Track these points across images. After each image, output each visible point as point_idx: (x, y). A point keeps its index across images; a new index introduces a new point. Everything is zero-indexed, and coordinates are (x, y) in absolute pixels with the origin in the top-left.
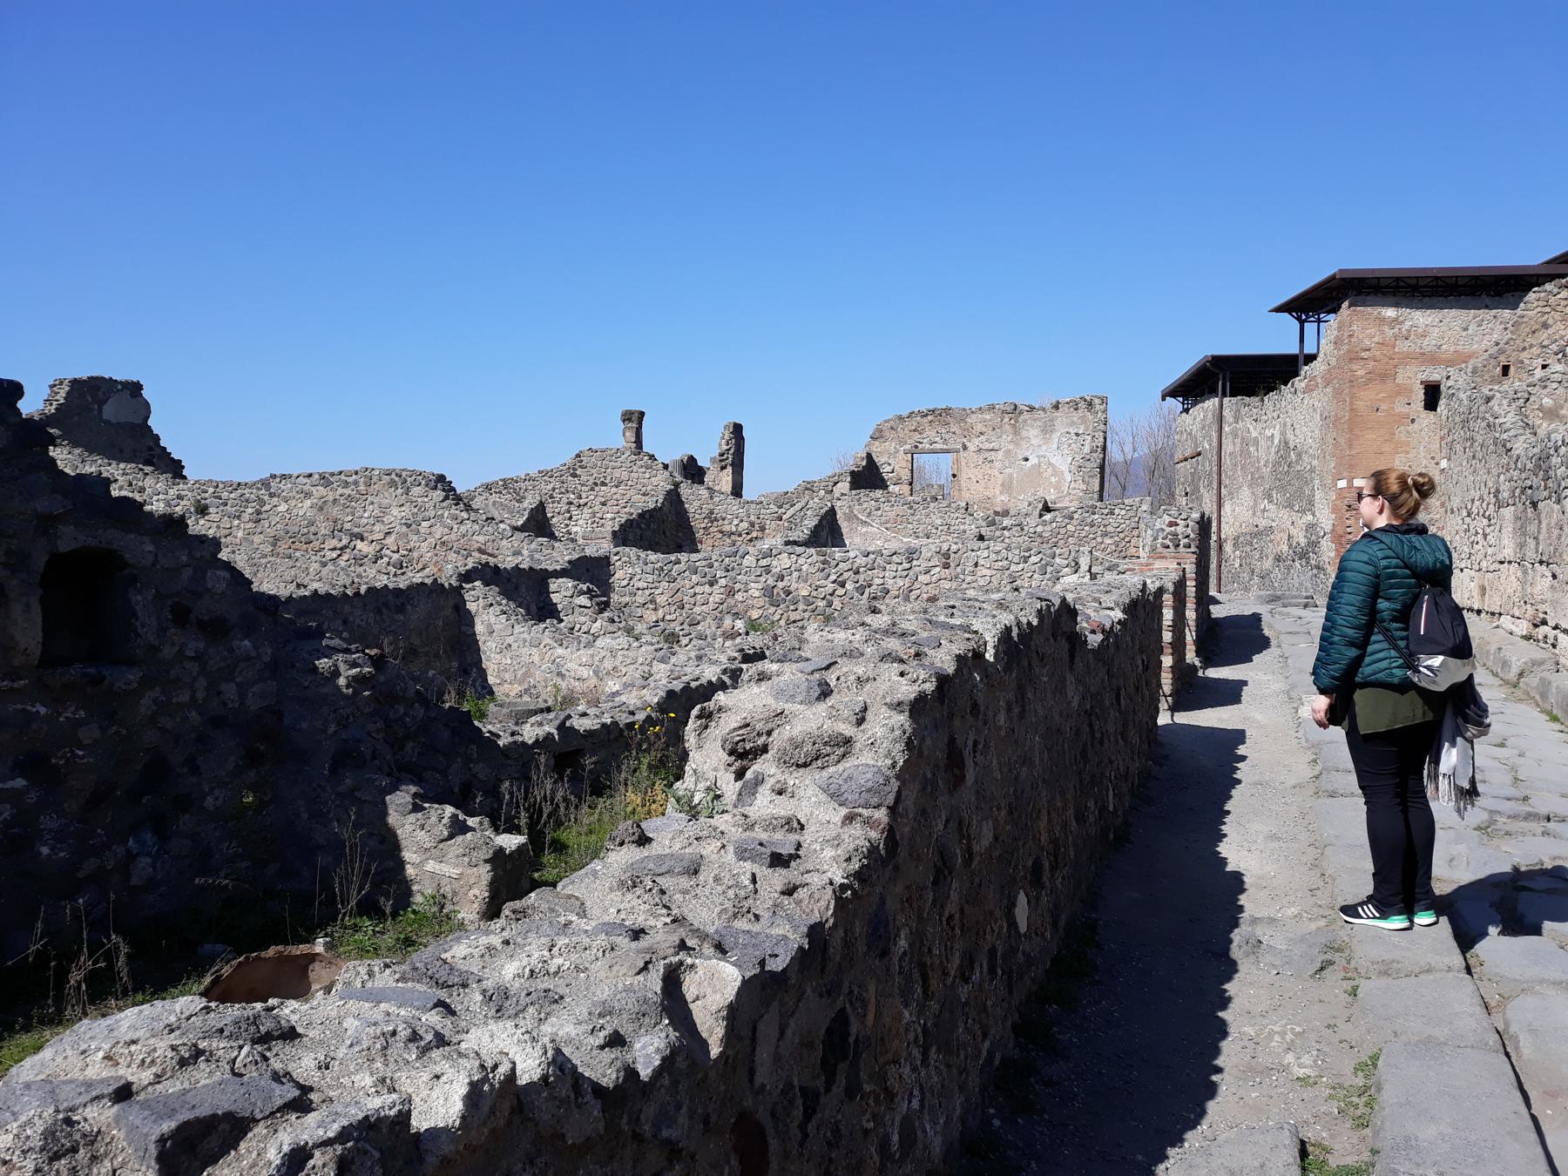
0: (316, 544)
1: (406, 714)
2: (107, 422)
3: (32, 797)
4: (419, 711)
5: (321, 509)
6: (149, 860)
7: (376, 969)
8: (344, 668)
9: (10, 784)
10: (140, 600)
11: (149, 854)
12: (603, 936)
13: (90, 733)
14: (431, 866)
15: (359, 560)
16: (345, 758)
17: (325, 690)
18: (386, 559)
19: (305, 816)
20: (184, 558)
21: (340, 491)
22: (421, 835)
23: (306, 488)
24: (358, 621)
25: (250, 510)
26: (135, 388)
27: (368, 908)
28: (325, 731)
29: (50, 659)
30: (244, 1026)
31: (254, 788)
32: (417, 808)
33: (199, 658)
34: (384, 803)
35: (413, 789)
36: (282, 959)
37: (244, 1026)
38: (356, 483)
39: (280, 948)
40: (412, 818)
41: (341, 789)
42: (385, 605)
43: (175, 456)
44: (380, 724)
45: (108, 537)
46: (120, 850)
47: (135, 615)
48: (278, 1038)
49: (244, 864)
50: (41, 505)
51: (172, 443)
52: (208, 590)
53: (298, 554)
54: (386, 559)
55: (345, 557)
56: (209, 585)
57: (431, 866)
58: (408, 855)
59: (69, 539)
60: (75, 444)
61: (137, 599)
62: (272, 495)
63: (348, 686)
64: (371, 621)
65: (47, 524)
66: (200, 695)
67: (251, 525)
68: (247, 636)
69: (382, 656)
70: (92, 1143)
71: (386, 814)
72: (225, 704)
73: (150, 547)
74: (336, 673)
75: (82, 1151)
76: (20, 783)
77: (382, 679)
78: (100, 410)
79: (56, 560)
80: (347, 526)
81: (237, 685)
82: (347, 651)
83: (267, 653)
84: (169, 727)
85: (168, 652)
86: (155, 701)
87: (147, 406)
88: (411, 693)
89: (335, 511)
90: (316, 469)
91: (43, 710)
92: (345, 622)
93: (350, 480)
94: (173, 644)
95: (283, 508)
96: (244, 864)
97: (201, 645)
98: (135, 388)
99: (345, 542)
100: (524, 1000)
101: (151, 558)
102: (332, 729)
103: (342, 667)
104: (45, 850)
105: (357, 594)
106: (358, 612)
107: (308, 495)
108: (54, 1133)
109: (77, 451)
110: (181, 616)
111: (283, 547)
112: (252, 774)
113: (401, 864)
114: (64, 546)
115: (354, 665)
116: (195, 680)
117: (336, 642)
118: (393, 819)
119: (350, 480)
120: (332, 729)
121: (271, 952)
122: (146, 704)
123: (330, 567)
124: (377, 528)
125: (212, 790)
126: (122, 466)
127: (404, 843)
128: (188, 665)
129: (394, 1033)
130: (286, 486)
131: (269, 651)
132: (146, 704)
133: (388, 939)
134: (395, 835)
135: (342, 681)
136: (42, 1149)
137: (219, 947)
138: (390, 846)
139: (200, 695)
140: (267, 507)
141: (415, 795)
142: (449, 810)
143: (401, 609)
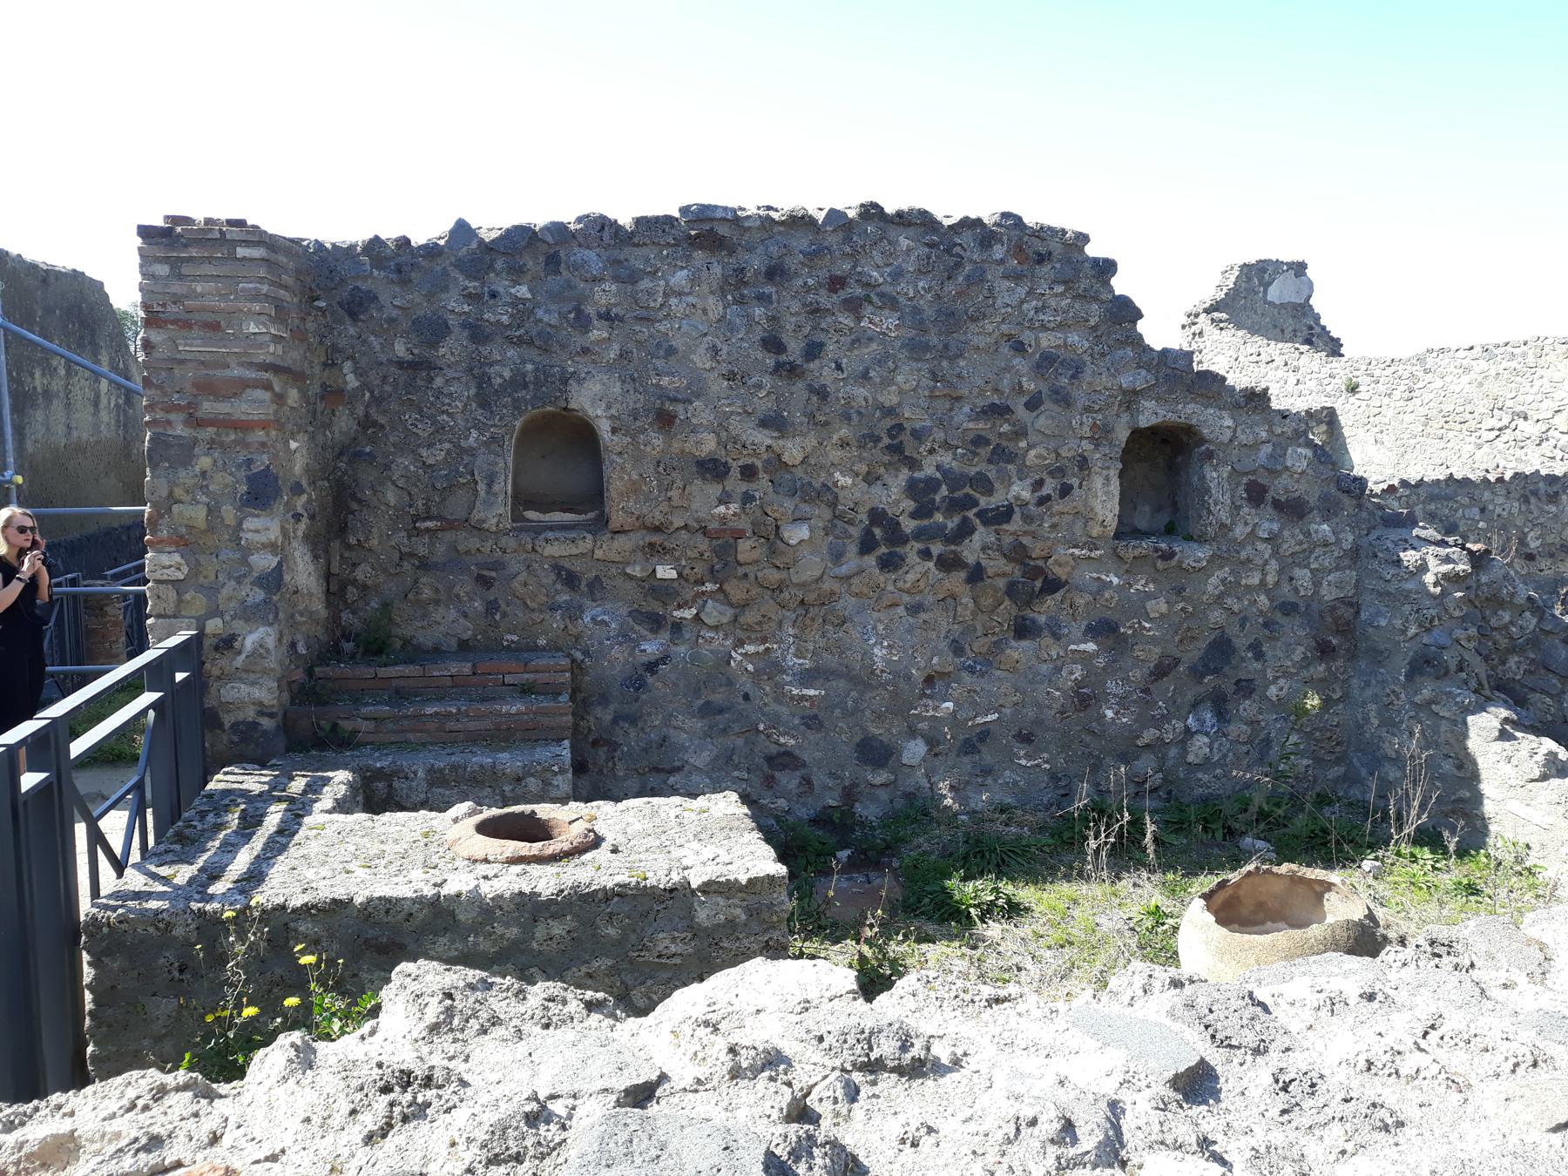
0: (1472, 424)
1: (1511, 622)
2: (1271, 303)
3: (1101, 662)
4: (1530, 621)
5: (1481, 384)
6: (1206, 740)
7: (1157, 984)
8: (1433, 562)
9: (1082, 647)
10: (1215, 477)
11: (1207, 734)
12: (1533, 1033)
13: (1158, 606)
14: (1514, 806)
15: (1520, 444)
16: (1425, 664)
17: (1409, 586)
18: (1552, 442)
19: (1376, 722)
20: (1264, 434)
21: (1505, 364)
22: (1508, 769)
23: (1465, 362)
24: (1499, 510)
25: (1402, 388)
26: (1300, 268)
27: (1429, 838)
28: (1404, 632)
29: (1126, 531)
30: (851, 1040)
31: (1321, 685)
32: (1504, 736)
33: (1272, 539)
34: (1465, 723)
35: (1504, 713)
36: (1294, 879)
37: (851, 1040)
38: (1524, 355)
39: (1294, 867)
40: (1499, 745)
41: (1418, 699)
42: (1535, 493)
43: (1334, 334)
44: (1473, 631)
45: (1190, 412)
46: (1179, 725)
47: (1208, 491)
48: (892, 1070)
49: (1305, 762)
50: (1125, 381)
51: (1332, 322)
52: (1287, 468)
53: (1451, 434)
54: (1552, 442)
55: (1504, 438)
56: (1289, 464)
57: (1514, 806)
58: (1486, 787)
59: (1150, 414)
60: (1239, 327)
61: (1211, 474)
62: (1427, 371)
63: (1436, 584)
64: (1515, 511)
65: (1130, 399)
66: (1271, 579)
67: (1402, 403)
68: (1326, 520)
69: (1488, 552)
70: (543, 1157)
71: (1465, 736)
72: (1296, 590)
73: (1229, 422)
74: (1423, 568)
75: (527, 1164)
76: (1091, 647)
77: (1484, 579)
78: (1265, 292)
79: (1137, 434)
80: (1509, 403)
81: (1312, 571)
82: (1442, 544)
83: (1348, 539)
84: (1236, 608)
85: (1240, 532)
86: (1223, 581)
87: (1310, 284)
88: (1520, 599)
89: (1494, 388)
90: (1477, 342)
91: (1115, 581)
92: (1483, 510)
93: (1516, 351)
94: (1246, 524)
95: (1439, 383)
96: (1305, 762)
97: (1275, 527)
98: (1300, 268)
99: (1505, 422)
100: (1337, 1108)
101: (1229, 434)
102: (1413, 631)
103: (1432, 562)
104: (1110, 714)
105: (1500, 480)
106: (1501, 500)
107: (1467, 370)
108: (504, 1130)
109: (1241, 333)
110: (1256, 494)
111: (1436, 425)
112: (1322, 668)
113: (1478, 798)
114: (1144, 422)
115: (1447, 560)
116: (1266, 563)
117: (1431, 533)
118: (1475, 744)
119: (1516, 351)
120: (1413, 631)
121: (1285, 868)
122: (1213, 584)
123: (1486, 448)
124: (1544, 405)
125: (1277, 678)
126: (1280, 345)
127: (1484, 774)
128: (1261, 546)
129: (1033, 1122)
130: (1444, 360)
131: (1351, 538)
132: (1213, 584)
133: (1447, 880)
134: (1475, 763)
135: (1429, 578)
136: (484, 1146)
137: (1260, 844)
138: (1468, 774)
139: (1271, 579)
140: (1421, 384)
141: (1506, 721)
142: (1549, 744)
143: (1553, 498)
